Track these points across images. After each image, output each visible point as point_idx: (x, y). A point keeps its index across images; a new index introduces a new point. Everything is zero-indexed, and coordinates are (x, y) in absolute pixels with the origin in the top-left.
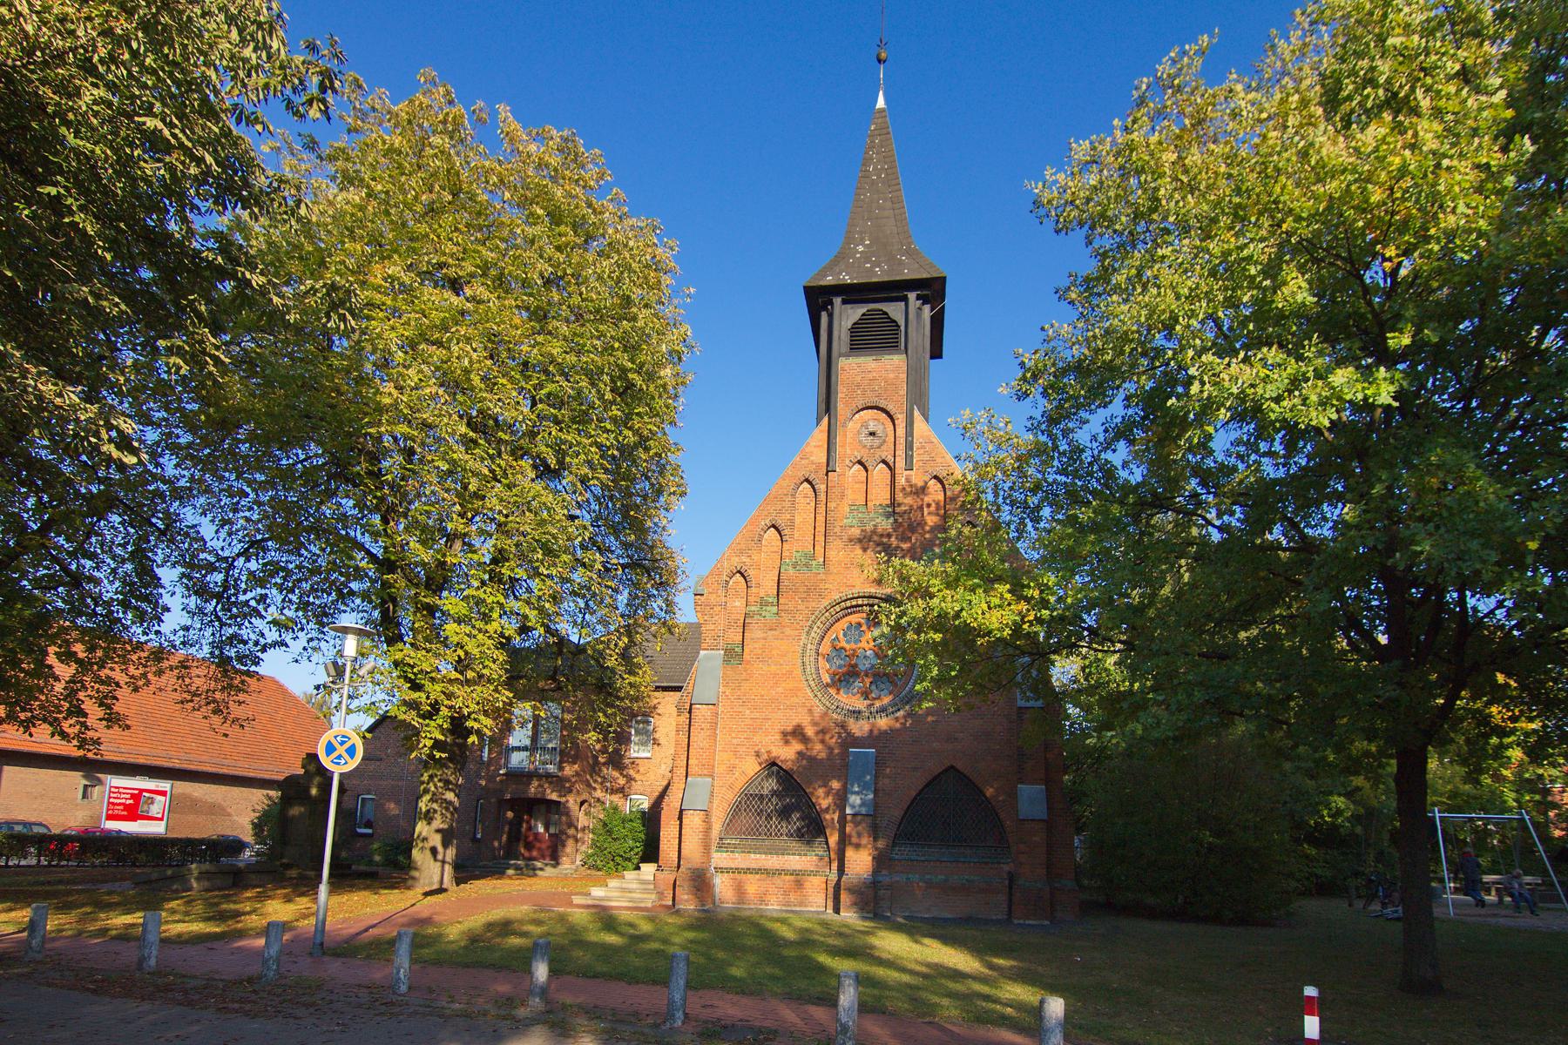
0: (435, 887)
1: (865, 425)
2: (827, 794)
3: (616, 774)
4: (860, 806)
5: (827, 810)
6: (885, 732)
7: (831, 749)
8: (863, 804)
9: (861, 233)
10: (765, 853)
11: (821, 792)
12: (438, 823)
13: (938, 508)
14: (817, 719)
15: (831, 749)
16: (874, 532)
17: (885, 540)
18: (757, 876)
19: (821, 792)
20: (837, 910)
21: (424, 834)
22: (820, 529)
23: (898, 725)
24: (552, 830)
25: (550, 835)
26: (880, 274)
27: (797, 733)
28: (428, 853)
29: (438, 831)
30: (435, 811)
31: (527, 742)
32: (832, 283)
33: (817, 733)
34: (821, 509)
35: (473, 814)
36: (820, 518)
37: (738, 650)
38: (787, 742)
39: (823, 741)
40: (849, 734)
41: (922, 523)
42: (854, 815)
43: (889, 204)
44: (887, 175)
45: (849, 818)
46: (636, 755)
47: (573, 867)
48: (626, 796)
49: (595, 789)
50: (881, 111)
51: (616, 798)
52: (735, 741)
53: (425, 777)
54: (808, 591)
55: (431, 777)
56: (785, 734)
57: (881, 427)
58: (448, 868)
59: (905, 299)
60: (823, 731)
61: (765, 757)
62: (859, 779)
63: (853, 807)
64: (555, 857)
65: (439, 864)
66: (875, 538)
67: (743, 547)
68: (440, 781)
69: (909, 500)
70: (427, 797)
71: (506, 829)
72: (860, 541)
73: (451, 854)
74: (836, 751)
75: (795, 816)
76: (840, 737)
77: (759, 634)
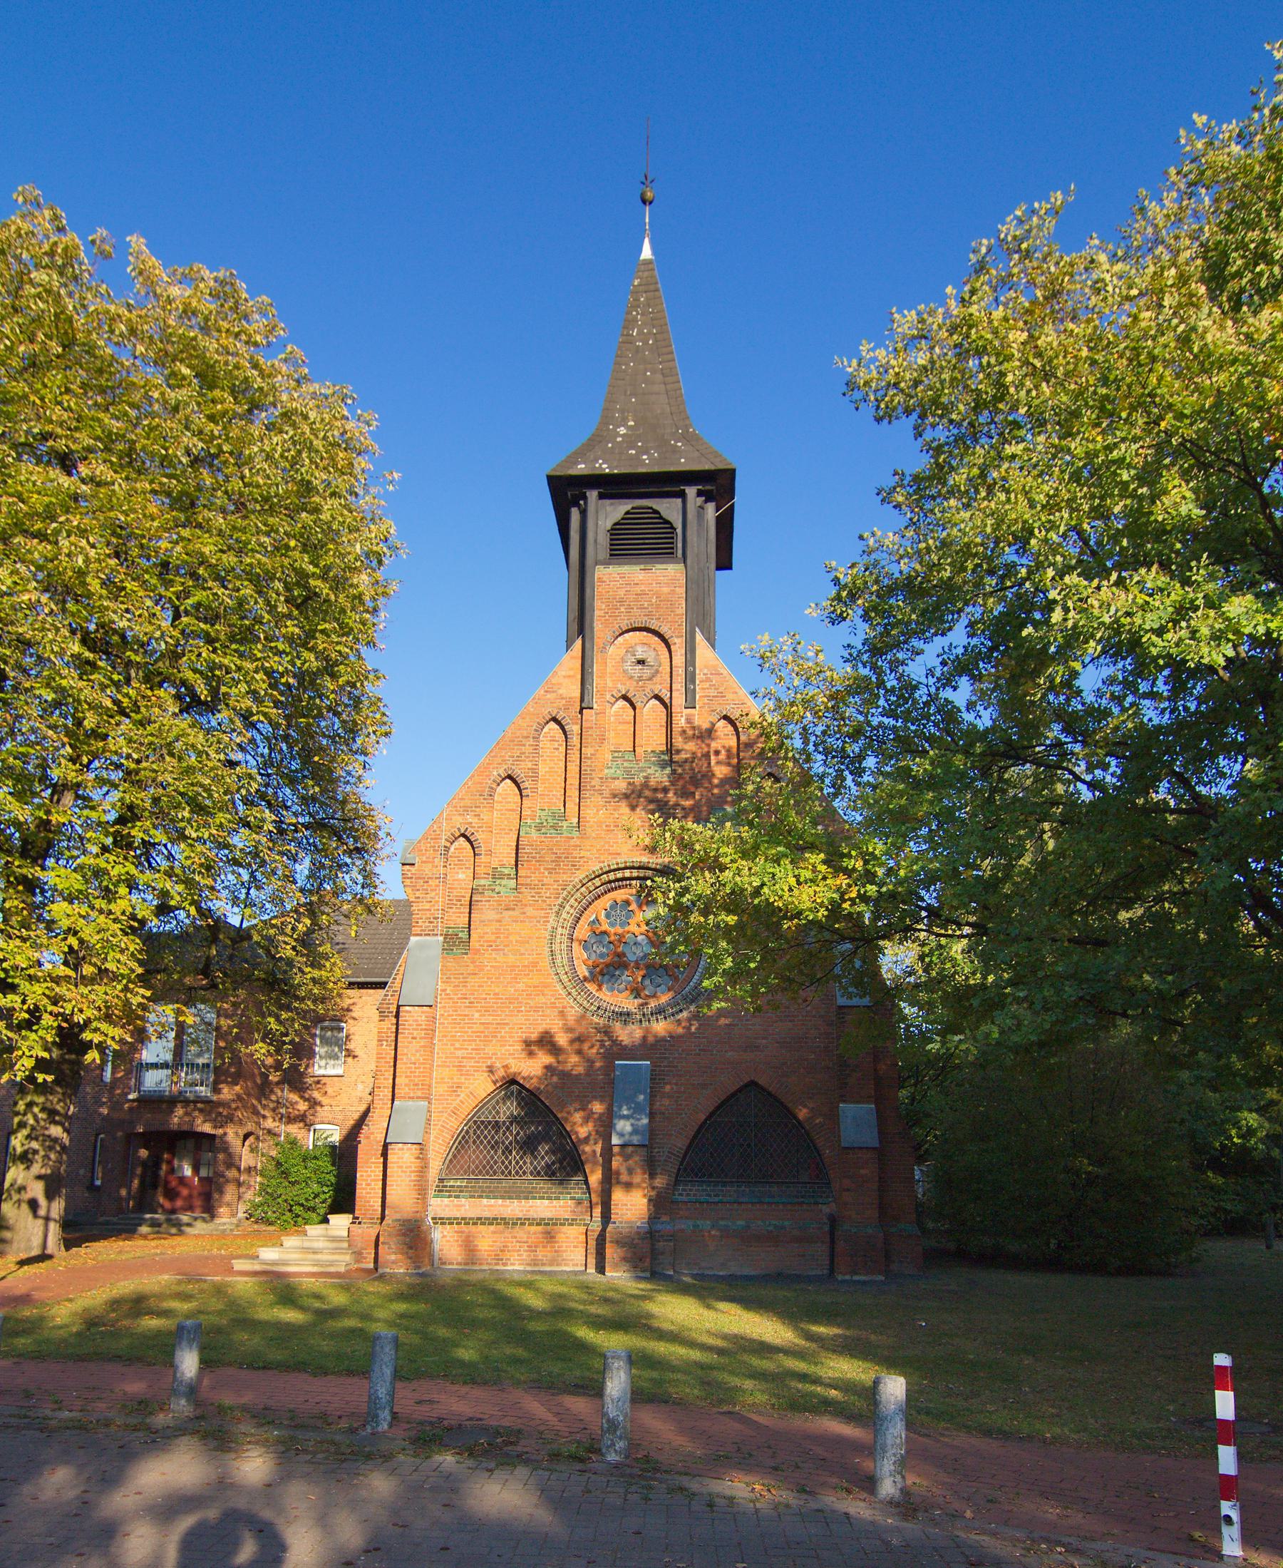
0: (35, 1252)
1: (631, 650)
2: (586, 1120)
3: (294, 1097)
4: (631, 1134)
5: (586, 1140)
6: (663, 1039)
7: (590, 1062)
8: (635, 1131)
9: (622, 411)
10: (503, 1198)
11: (578, 1117)
12: (36, 1169)
13: (729, 756)
14: (571, 1023)
15: (590, 1062)
16: (645, 785)
17: (660, 796)
18: (492, 1228)
19: (578, 1117)
20: (601, 1269)
21: (19, 1182)
22: (573, 781)
23: (680, 1030)
24: (203, 1173)
25: (200, 1179)
26: (648, 463)
27: (546, 1042)
28: (25, 1207)
29: (39, 1177)
30: (35, 1152)
31: (168, 1057)
32: (585, 472)
33: (572, 1042)
34: (574, 756)
35: (90, 1154)
36: (573, 768)
37: (464, 935)
38: (531, 1054)
39: (579, 1052)
40: (615, 1042)
41: (709, 775)
42: (623, 1146)
43: (659, 377)
44: (656, 341)
45: (616, 1150)
46: (322, 1072)
47: (234, 1220)
48: (308, 1126)
49: (264, 1117)
50: (647, 262)
51: (295, 1130)
52: (459, 1053)
53: (21, 1106)
54: (557, 860)
55: (30, 1105)
56: (528, 1043)
57: (653, 654)
58: (54, 1228)
59: (682, 495)
60: (580, 1039)
61: (501, 1073)
62: (629, 1100)
63: (621, 1135)
64: (210, 1210)
65: (40, 1222)
66: (647, 793)
67: (468, 803)
68: (43, 1110)
69: (691, 746)
70: (25, 1132)
71: (139, 1171)
72: (626, 796)
73: (58, 1208)
74: (598, 1064)
75: (543, 1148)
76: (602, 1046)
77: (492, 915)
